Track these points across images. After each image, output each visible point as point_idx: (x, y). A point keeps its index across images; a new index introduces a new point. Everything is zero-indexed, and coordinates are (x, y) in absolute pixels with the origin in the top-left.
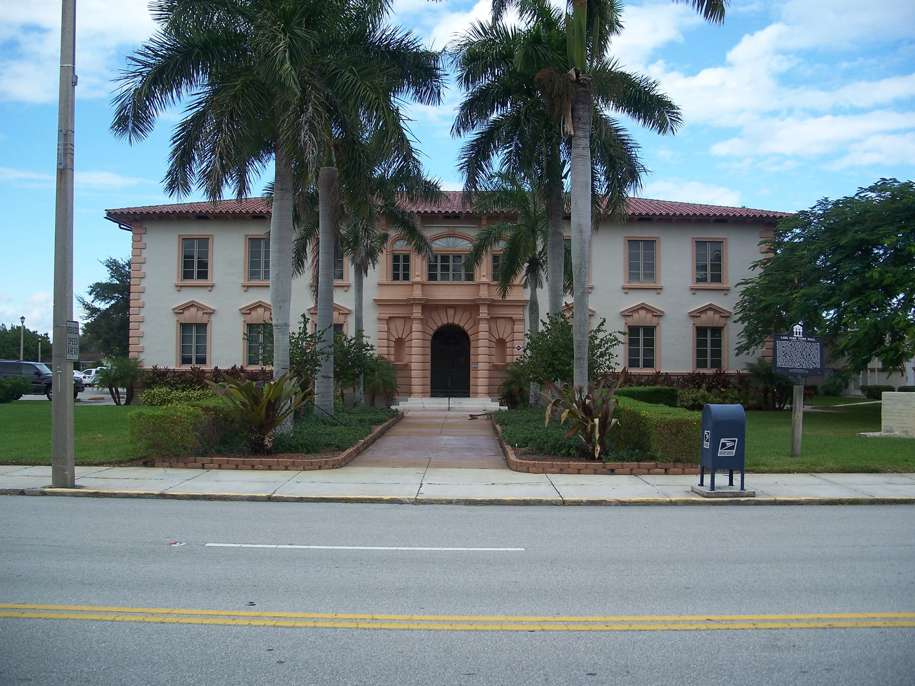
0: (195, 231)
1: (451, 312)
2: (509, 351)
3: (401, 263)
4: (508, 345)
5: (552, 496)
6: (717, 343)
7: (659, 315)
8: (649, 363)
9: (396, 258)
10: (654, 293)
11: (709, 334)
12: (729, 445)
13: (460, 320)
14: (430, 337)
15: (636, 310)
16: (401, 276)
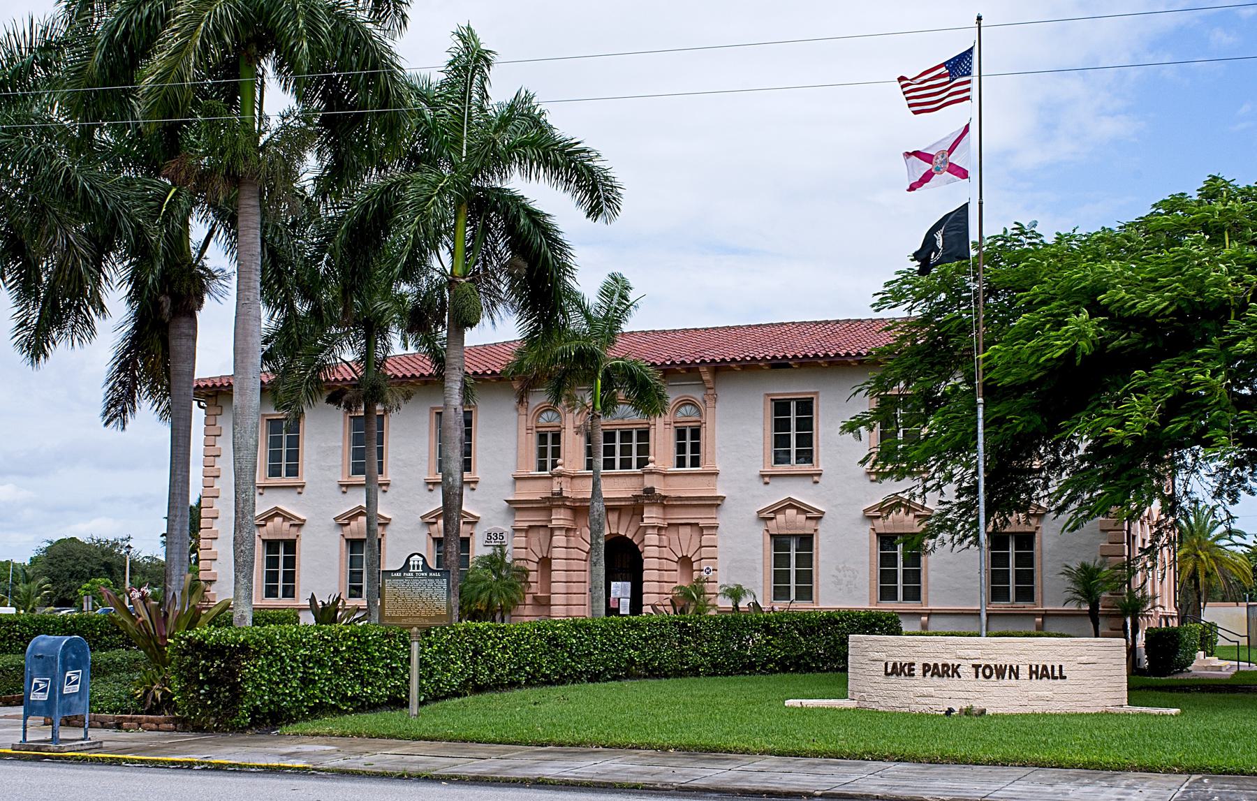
3: (688, 442)
4: (695, 566)
6: (1026, 560)
8: (805, 593)
9: (681, 434)
11: (282, 550)
12: (42, 686)
13: (625, 529)
16: (688, 462)
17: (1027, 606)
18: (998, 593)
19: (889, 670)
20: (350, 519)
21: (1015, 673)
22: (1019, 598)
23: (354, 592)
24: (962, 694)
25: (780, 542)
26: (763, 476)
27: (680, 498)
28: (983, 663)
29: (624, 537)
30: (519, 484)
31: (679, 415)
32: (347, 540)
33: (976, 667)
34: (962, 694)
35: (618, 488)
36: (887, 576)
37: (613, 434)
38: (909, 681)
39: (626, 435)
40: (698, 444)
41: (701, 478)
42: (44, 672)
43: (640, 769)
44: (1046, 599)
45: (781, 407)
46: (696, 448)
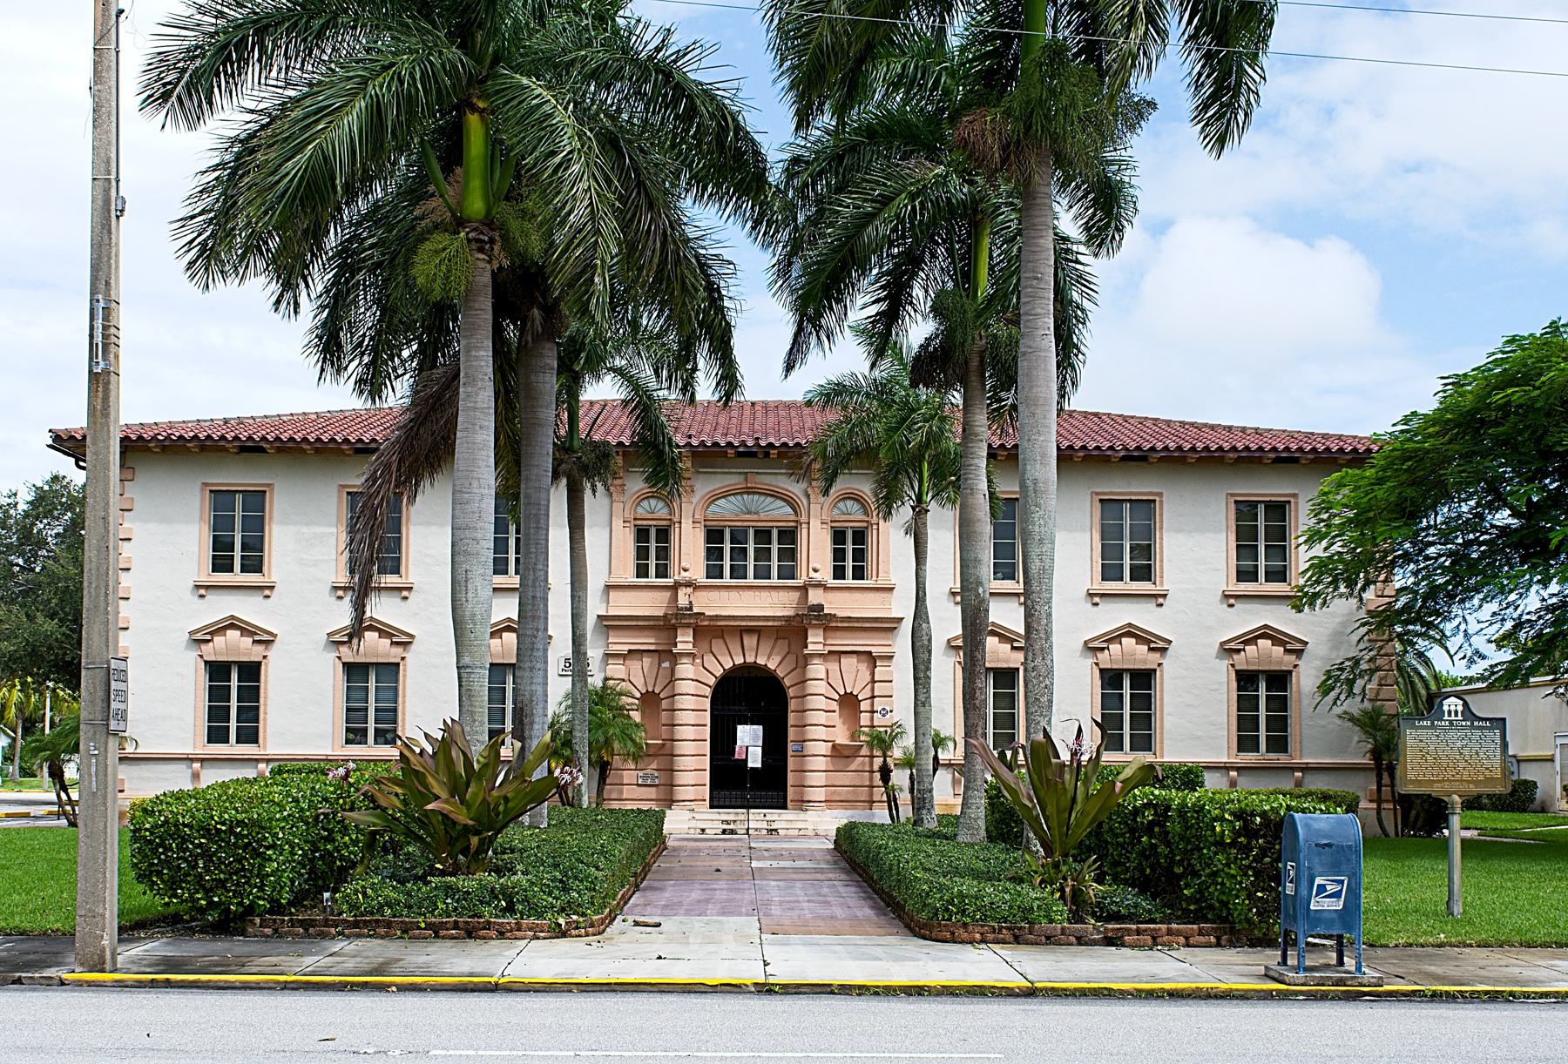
1: (750, 641)
2: (865, 719)
3: (849, 547)
4: (864, 706)
5: (752, 973)
6: (1279, 704)
7: (1160, 647)
8: (1143, 742)
10: (1150, 606)
11: (234, 676)
12: (1331, 888)
13: (770, 660)
14: (708, 692)
15: (220, 629)
16: (652, 570)
17: (1283, 759)
20: (1246, 643)
23: (351, 736)
25: (218, 671)
26: (1091, 595)
27: (849, 619)
29: (735, 668)
31: (640, 510)
35: (765, 603)
36: (217, 714)
37: (721, 533)
39: (763, 535)
41: (871, 595)
42: (1334, 868)
43: (1508, 970)
44: (1305, 751)
45: (1245, 510)
46: (859, 555)
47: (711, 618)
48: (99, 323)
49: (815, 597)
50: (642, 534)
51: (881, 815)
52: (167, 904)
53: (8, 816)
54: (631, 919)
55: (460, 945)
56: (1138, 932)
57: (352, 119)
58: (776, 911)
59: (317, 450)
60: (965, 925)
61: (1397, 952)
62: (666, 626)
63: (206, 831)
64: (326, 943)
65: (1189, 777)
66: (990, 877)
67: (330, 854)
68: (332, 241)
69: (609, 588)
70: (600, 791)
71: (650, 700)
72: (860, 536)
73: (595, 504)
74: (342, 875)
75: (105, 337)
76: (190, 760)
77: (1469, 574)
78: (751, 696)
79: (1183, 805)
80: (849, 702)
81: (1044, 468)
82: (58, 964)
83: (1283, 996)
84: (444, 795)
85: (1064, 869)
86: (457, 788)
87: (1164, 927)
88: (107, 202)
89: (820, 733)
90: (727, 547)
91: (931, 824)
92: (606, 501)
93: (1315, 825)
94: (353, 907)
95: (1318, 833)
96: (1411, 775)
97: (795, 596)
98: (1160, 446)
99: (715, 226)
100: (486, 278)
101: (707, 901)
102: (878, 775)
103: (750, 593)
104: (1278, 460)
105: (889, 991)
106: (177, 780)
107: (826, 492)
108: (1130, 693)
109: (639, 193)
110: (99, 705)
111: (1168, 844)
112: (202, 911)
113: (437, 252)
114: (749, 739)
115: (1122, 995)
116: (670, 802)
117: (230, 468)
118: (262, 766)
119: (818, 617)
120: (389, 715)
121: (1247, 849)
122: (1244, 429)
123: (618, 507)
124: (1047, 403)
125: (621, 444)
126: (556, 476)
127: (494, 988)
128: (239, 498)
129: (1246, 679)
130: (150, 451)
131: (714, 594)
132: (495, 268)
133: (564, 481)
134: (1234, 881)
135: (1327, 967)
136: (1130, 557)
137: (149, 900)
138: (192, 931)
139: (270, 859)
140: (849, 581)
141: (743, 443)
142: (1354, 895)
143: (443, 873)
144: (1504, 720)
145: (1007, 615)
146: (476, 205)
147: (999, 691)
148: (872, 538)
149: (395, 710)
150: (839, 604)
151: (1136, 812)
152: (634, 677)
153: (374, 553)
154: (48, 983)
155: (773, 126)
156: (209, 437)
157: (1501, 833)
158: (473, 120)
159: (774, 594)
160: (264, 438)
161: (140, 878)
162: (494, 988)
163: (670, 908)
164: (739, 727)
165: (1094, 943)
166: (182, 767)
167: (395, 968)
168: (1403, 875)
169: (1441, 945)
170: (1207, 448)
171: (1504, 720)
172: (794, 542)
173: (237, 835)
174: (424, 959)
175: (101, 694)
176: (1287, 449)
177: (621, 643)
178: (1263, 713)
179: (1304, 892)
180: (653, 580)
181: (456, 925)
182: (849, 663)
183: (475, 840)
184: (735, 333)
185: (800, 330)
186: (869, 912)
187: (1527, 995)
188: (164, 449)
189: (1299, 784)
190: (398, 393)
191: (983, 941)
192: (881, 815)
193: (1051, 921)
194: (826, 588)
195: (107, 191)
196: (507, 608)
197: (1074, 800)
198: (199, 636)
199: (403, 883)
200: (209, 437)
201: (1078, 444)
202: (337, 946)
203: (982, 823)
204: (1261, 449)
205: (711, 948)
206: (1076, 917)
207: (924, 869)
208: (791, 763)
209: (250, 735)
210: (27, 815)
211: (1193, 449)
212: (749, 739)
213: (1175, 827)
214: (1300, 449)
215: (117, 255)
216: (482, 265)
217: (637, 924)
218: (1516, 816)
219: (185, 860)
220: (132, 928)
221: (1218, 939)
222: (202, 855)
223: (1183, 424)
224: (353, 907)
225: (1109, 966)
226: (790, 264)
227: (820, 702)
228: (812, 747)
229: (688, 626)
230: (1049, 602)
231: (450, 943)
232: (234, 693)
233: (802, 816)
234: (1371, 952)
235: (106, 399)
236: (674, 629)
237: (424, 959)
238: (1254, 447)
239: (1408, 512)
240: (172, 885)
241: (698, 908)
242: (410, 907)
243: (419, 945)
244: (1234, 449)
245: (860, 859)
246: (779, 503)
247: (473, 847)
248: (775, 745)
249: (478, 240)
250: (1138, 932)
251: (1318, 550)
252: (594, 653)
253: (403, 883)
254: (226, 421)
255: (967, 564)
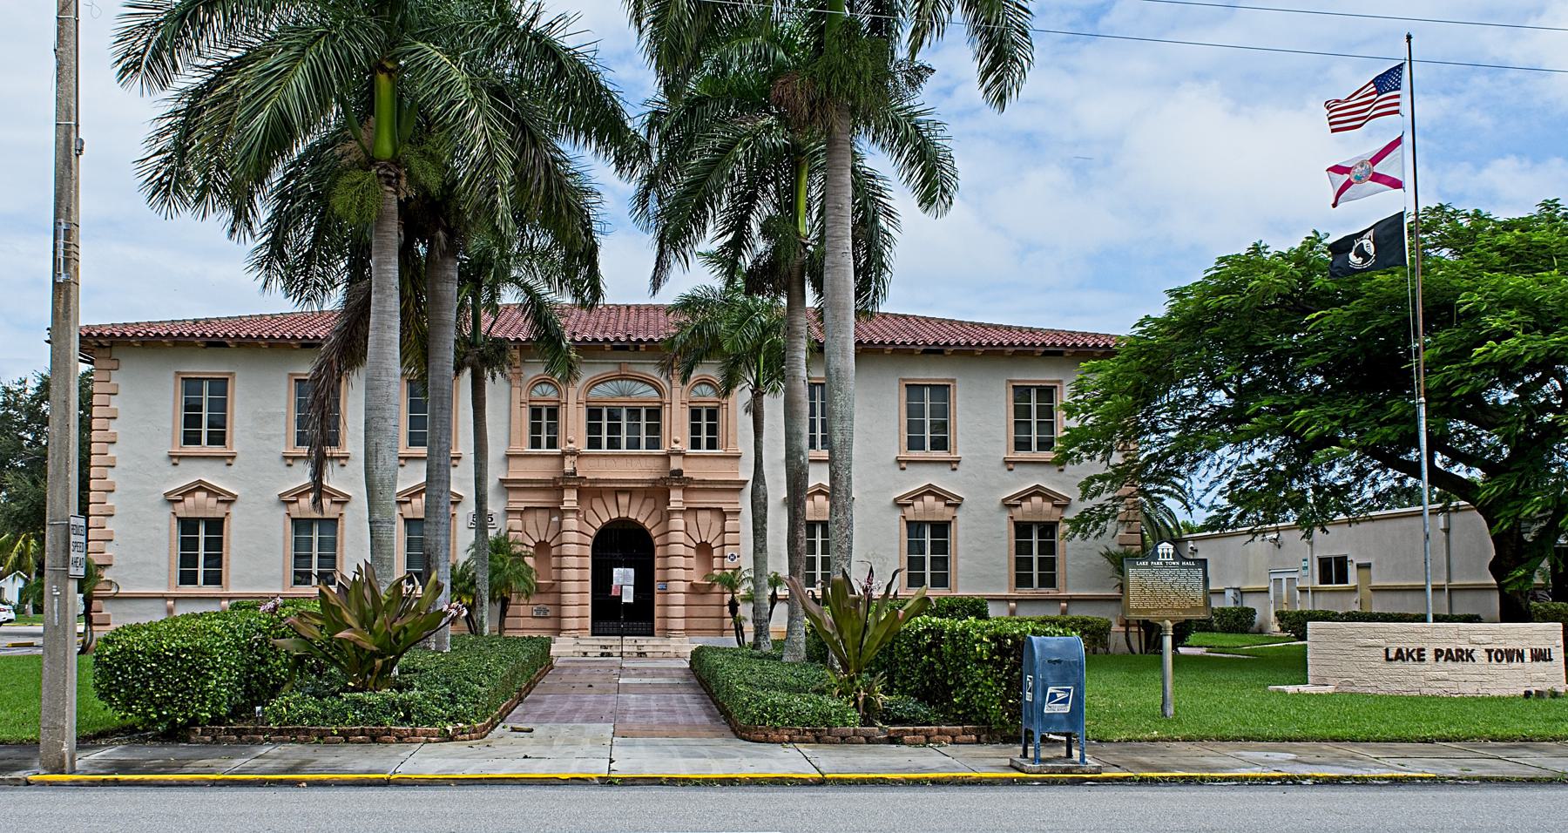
0: (204, 367)
1: (624, 500)
2: (716, 562)
3: (704, 423)
4: (716, 552)
5: (600, 768)
8: (941, 580)
12: (1061, 696)
13: (638, 513)
14: (590, 541)
15: (189, 491)
17: (1051, 592)
18: (1023, 580)
19: (1392, 655)
20: (1022, 499)
21: (1521, 656)
22: (208, 581)
24: (1477, 678)
27: (711, 482)
28: (1495, 647)
29: (612, 522)
30: (512, 462)
32: (293, 520)
33: (1489, 651)
34: (1477, 678)
35: (636, 468)
38: (1419, 667)
39: (634, 413)
40: (556, 425)
41: (721, 462)
42: (1062, 680)
45: (1021, 392)
46: (712, 430)
47: (591, 481)
48: (61, 241)
49: (676, 463)
50: (536, 413)
51: (731, 641)
52: (124, 717)
53: (14, 645)
54: (509, 726)
55: (365, 748)
56: (915, 733)
57: (299, 79)
58: (629, 718)
59: (271, 345)
60: (776, 728)
61: (1119, 746)
62: (555, 488)
63: (156, 657)
64: (255, 748)
65: (977, 608)
66: (798, 690)
67: (264, 675)
68: (276, 177)
69: (509, 457)
70: (502, 623)
71: (542, 547)
72: (713, 414)
73: (495, 389)
74: (274, 691)
75: (66, 253)
76: (164, 598)
77: (1193, 444)
78: (624, 544)
79: (953, 630)
80: (704, 549)
81: (846, 360)
82: (26, 768)
83: (1023, 782)
84: (355, 625)
85: (858, 682)
86: (365, 622)
87: (935, 728)
88: (68, 143)
89: (681, 574)
90: (605, 423)
91: (767, 648)
92: (507, 386)
93: (1049, 646)
94: (279, 718)
95: (1050, 651)
96: (1133, 605)
97: (659, 462)
98: (953, 341)
99: (589, 163)
100: (394, 207)
101: (576, 711)
102: (727, 608)
103: (623, 462)
104: (1047, 354)
105: (708, 782)
106: (154, 614)
107: (685, 380)
108: (930, 541)
109: (524, 135)
110: (60, 556)
111: (942, 662)
112: (153, 722)
113: (353, 185)
114: (623, 579)
115: (894, 783)
116: (559, 631)
117: (202, 356)
118: (225, 603)
119: (678, 480)
120: (329, 560)
121: (1000, 665)
122: (1020, 329)
123: (516, 391)
124: (846, 308)
125: (518, 340)
126: (458, 369)
127: (386, 783)
128: (206, 385)
129: (1022, 529)
130: (105, 346)
131: (594, 462)
132: (402, 197)
133: (468, 371)
134: (989, 692)
135: (1060, 757)
136: (929, 431)
137: (113, 716)
138: (146, 739)
139: (212, 678)
140: (704, 451)
141: (617, 339)
142: (1078, 699)
143: (354, 690)
144: (1205, 561)
145: (818, 477)
146: (385, 148)
147: (815, 539)
148: (722, 415)
149: (334, 557)
150: (693, 470)
151: (918, 636)
152: (525, 533)
153: (318, 429)
154: (16, 783)
155: (636, 84)
156: (181, 334)
157: (1223, 649)
158: (383, 79)
159: (643, 461)
160: (226, 335)
161: (101, 696)
162: (386, 783)
163: (544, 717)
164: (615, 570)
165: (880, 742)
166: (159, 604)
167: (308, 767)
168: (1138, 685)
169: (1154, 740)
170: (990, 344)
171: (1205, 561)
172: (659, 418)
173: (182, 660)
174: (333, 759)
175: (61, 545)
176: (1054, 344)
177: (520, 501)
178: (928, 555)
179: (1039, 699)
180: (544, 450)
181: (363, 732)
182: (704, 517)
183: (379, 662)
184: (601, 251)
185: (661, 252)
186: (705, 719)
187: (1214, 780)
188: (144, 344)
189: (1064, 612)
190: (335, 300)
191: (791, 741)
192: (731, 641)
193: (845, 725)
194: (685, 456)
195: (68, 134)
196: (415, 476)
197: (866, 627)
198: (172, 497)
199: (320, 698)
200: (181, 334)
201: (888, 341)
202: (263, 750)
203: (803, 646)
204: (1033, 344)
205: (570, 749)
206: (867, 721)
207: (747, 684)
208: (658, 599)
209: (214, 578)
210: (31, 645)
211: (979, 344)
212: (623, 579)
213: (947, 648)
214: (1064, 345)
215: (77, 186)
216: (390, 195)
217: (513, 730)
218: (1239, 636)
219: (139, 680)
220: (86, 741)
221: (978, 737)
222: (153, 677)
223: (973, 324)
224: (279, 718)
225: (887, 760)
226: (647, 195)
227: (681, 549)
228: (673, 586)
229: (572, 487)
230: (849, 468)
231: (357, 746)
232: (201, 542)
233: (666, 642)
234: (1098, 747)
235: (67, 303)
236: (562, 490)
237: (333, 759)
238: (1027, 343)
239: (1145, 396)
240: (128, 703)
241: (567, 717)
242: (325, 718)
243: (332, 748)
244: (1012, 344)
245: (705, 676)
246: (648, 387)
247: (377, 669)
248: (644, 584)
249: (386, 176)
250: (915, 733)
251: (1074, 423)
252: (494, 506)
253: (320, 698)
254: (196, 321)
255: (791, 436)
